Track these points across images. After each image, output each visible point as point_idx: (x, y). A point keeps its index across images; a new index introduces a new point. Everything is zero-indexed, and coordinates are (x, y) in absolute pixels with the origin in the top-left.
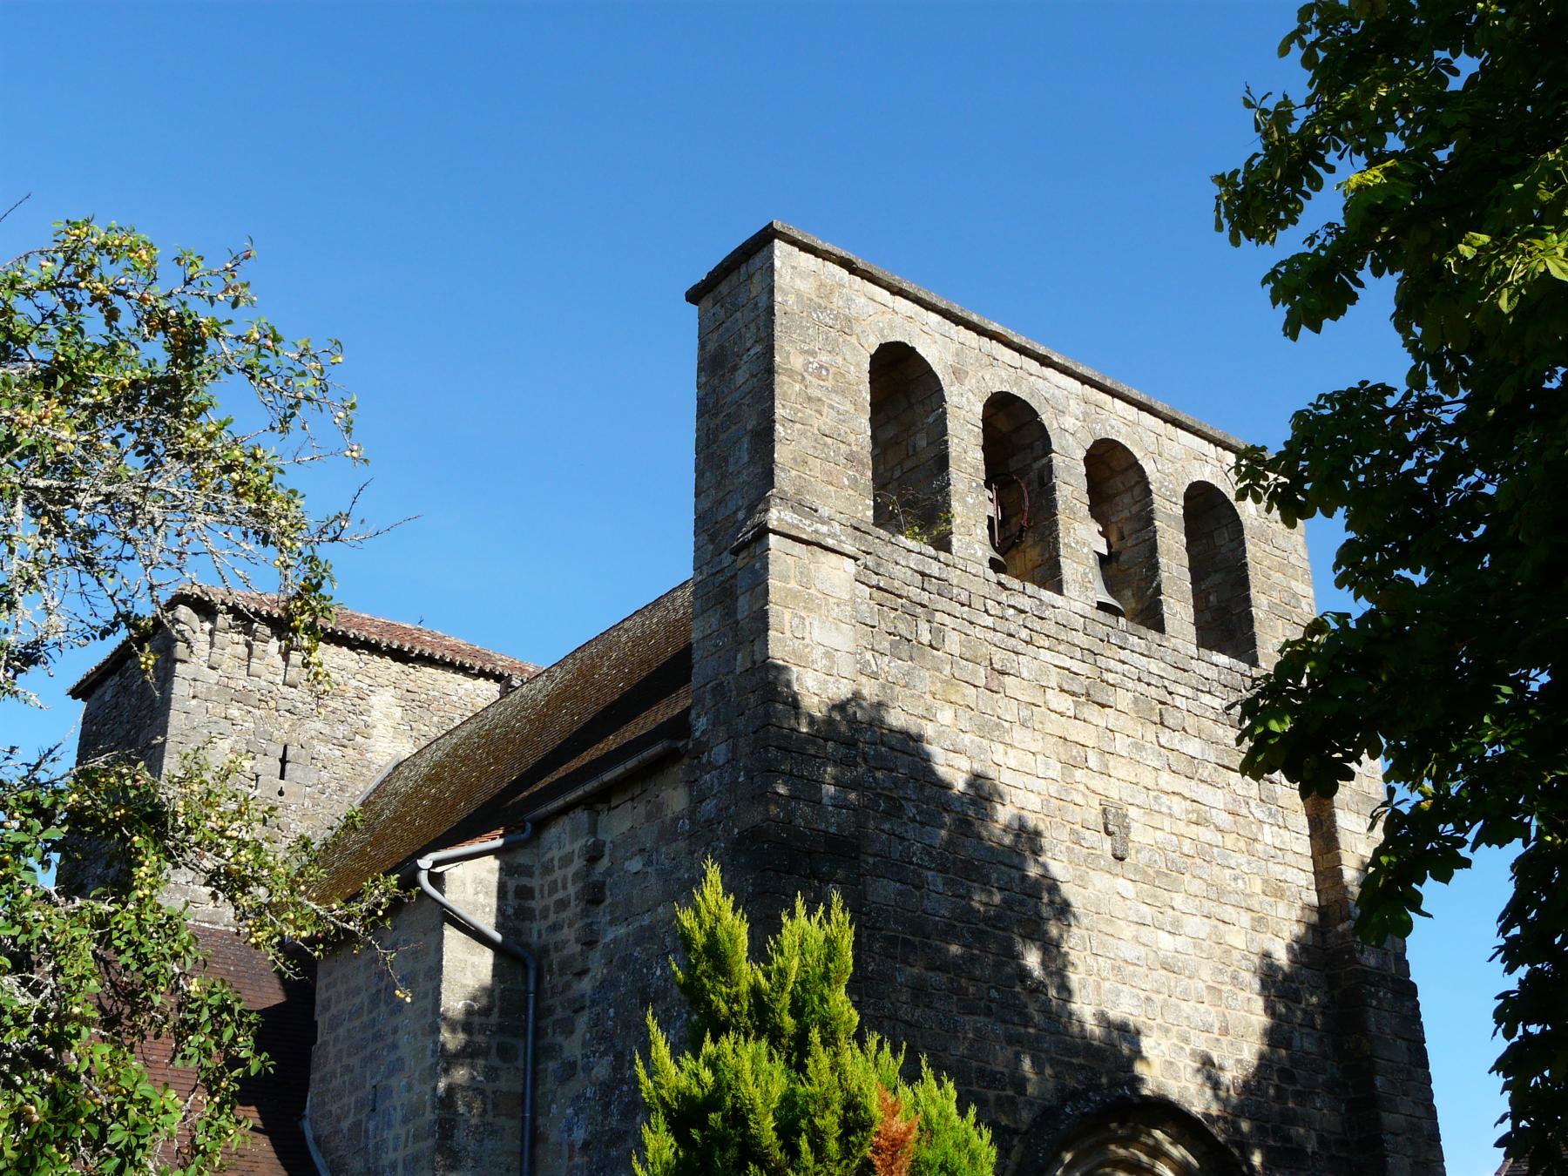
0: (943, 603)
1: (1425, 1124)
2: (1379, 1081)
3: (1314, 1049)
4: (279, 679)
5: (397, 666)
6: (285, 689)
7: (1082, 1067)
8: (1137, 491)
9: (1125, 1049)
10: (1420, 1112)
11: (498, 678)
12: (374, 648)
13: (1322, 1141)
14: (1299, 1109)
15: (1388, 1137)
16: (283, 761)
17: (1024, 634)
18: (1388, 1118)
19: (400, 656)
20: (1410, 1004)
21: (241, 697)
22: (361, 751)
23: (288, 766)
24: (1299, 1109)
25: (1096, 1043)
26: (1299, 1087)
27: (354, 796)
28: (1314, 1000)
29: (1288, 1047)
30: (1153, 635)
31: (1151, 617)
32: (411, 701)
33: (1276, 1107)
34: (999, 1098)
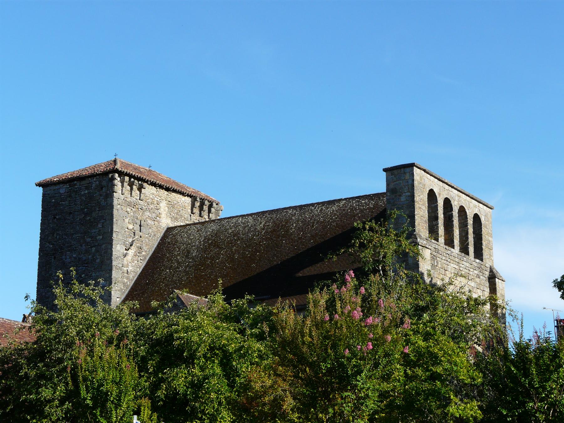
0: (438, 255)
4: (138, 198)
5: (166, 193)
6: (140, 201)
8: (463, 217)
11: (190, 196)
12: (161, 187)
16: (140, 226)
17: (449, 260)
19: (167, 189)
21: (129, 204)
22: (159, 222)
23: (142, 228)
27: (157, 238)
30: (467, 256)
31: (467, 253)
32: (171, 205)
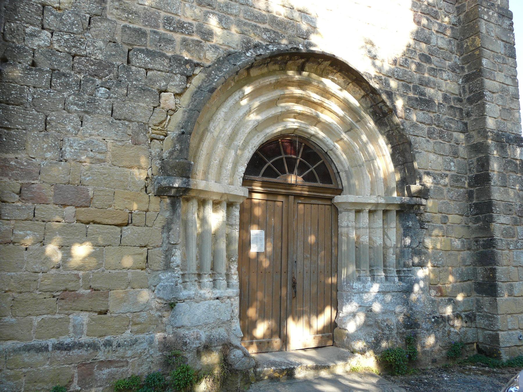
1: (511, 89)
2: (484, 61)
3: (445, 46)
7: (267, 30)
9: (304, 27)
10: (509, 81)
13: (445, 98)
14: (432, 78)
15: (488, 93)
18: (488, 83)
20: (508, 22)
24: (432, 78)
25: (419, 348)
26: (433, 66)
28: (447, 19)
29: (427, 42)
33: (417, 76)
34: (184, 40)
